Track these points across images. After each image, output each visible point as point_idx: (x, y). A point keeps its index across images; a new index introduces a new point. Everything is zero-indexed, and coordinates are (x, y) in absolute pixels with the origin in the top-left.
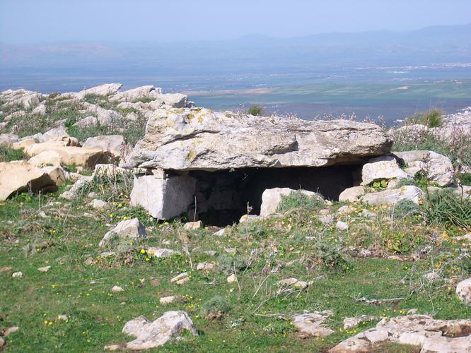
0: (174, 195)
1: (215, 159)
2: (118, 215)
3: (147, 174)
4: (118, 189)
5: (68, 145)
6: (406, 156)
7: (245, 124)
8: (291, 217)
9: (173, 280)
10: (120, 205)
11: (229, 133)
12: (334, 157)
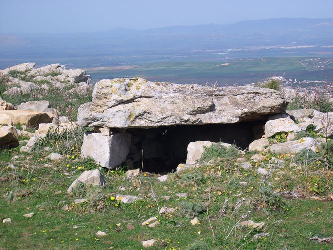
0: (118, 149)
1: (151, 119)
2: (73, 165)
3: (96, 132)
4: (69, 143)
5: (6, 109)
6: (297, 114)
7: (172, 91)
8: (219, 165)
9: (144, 224)
10: (73, 158)
11: (161, 98)
12: (244, 115)
